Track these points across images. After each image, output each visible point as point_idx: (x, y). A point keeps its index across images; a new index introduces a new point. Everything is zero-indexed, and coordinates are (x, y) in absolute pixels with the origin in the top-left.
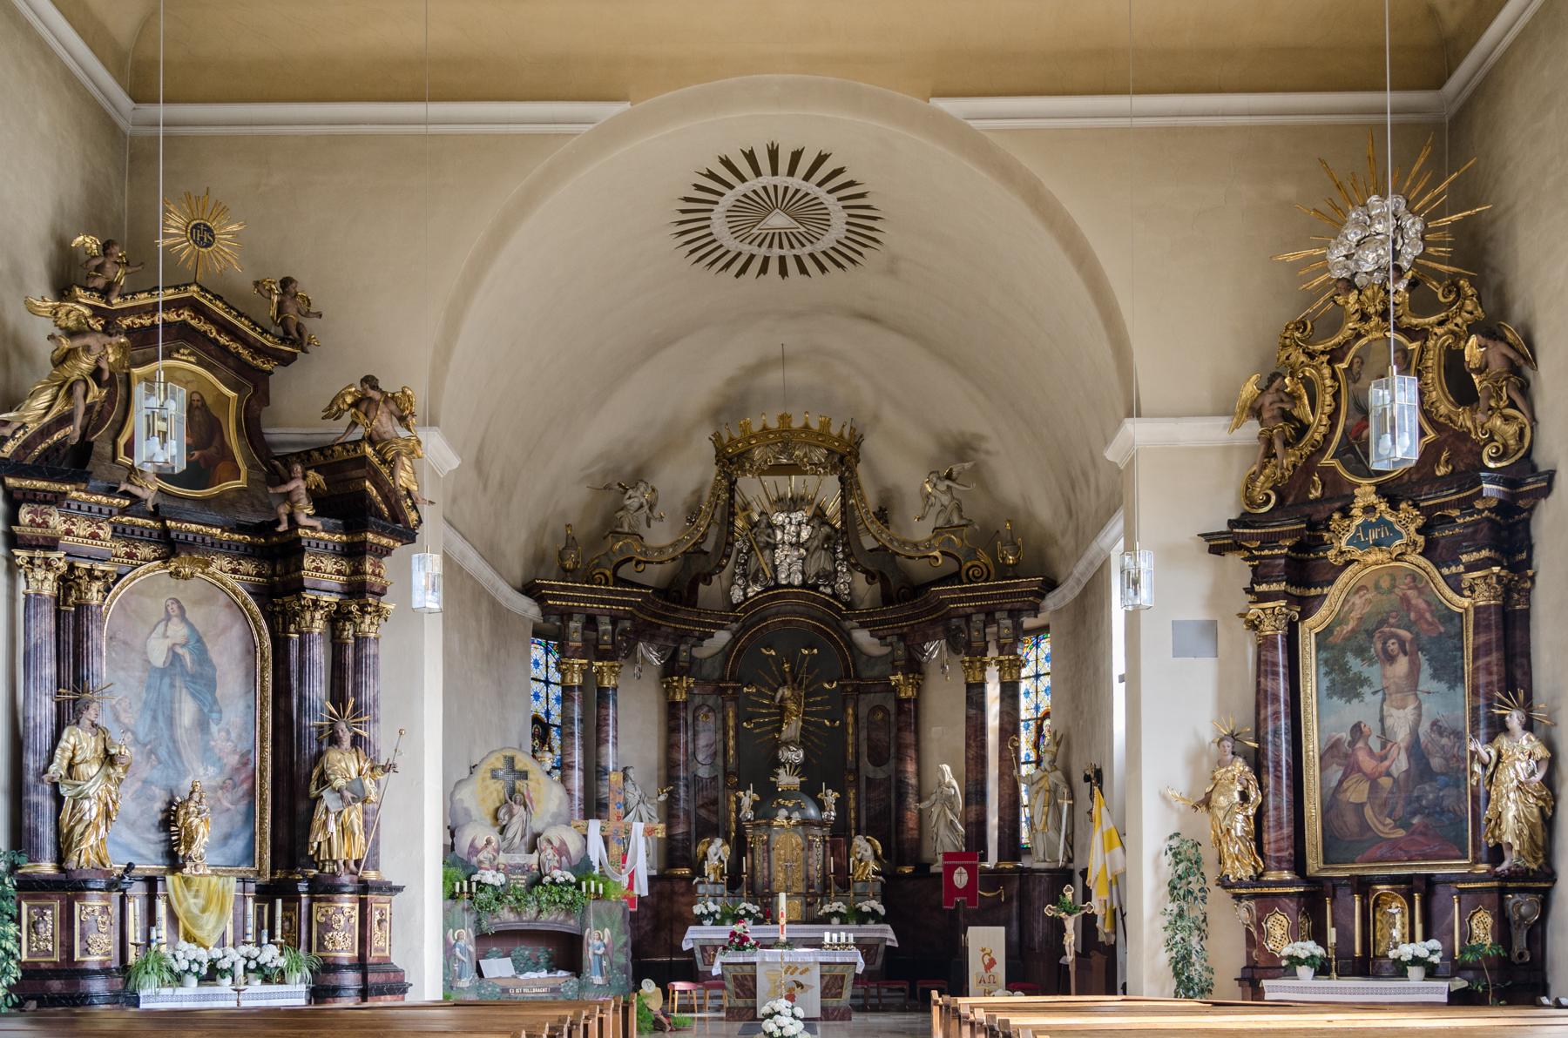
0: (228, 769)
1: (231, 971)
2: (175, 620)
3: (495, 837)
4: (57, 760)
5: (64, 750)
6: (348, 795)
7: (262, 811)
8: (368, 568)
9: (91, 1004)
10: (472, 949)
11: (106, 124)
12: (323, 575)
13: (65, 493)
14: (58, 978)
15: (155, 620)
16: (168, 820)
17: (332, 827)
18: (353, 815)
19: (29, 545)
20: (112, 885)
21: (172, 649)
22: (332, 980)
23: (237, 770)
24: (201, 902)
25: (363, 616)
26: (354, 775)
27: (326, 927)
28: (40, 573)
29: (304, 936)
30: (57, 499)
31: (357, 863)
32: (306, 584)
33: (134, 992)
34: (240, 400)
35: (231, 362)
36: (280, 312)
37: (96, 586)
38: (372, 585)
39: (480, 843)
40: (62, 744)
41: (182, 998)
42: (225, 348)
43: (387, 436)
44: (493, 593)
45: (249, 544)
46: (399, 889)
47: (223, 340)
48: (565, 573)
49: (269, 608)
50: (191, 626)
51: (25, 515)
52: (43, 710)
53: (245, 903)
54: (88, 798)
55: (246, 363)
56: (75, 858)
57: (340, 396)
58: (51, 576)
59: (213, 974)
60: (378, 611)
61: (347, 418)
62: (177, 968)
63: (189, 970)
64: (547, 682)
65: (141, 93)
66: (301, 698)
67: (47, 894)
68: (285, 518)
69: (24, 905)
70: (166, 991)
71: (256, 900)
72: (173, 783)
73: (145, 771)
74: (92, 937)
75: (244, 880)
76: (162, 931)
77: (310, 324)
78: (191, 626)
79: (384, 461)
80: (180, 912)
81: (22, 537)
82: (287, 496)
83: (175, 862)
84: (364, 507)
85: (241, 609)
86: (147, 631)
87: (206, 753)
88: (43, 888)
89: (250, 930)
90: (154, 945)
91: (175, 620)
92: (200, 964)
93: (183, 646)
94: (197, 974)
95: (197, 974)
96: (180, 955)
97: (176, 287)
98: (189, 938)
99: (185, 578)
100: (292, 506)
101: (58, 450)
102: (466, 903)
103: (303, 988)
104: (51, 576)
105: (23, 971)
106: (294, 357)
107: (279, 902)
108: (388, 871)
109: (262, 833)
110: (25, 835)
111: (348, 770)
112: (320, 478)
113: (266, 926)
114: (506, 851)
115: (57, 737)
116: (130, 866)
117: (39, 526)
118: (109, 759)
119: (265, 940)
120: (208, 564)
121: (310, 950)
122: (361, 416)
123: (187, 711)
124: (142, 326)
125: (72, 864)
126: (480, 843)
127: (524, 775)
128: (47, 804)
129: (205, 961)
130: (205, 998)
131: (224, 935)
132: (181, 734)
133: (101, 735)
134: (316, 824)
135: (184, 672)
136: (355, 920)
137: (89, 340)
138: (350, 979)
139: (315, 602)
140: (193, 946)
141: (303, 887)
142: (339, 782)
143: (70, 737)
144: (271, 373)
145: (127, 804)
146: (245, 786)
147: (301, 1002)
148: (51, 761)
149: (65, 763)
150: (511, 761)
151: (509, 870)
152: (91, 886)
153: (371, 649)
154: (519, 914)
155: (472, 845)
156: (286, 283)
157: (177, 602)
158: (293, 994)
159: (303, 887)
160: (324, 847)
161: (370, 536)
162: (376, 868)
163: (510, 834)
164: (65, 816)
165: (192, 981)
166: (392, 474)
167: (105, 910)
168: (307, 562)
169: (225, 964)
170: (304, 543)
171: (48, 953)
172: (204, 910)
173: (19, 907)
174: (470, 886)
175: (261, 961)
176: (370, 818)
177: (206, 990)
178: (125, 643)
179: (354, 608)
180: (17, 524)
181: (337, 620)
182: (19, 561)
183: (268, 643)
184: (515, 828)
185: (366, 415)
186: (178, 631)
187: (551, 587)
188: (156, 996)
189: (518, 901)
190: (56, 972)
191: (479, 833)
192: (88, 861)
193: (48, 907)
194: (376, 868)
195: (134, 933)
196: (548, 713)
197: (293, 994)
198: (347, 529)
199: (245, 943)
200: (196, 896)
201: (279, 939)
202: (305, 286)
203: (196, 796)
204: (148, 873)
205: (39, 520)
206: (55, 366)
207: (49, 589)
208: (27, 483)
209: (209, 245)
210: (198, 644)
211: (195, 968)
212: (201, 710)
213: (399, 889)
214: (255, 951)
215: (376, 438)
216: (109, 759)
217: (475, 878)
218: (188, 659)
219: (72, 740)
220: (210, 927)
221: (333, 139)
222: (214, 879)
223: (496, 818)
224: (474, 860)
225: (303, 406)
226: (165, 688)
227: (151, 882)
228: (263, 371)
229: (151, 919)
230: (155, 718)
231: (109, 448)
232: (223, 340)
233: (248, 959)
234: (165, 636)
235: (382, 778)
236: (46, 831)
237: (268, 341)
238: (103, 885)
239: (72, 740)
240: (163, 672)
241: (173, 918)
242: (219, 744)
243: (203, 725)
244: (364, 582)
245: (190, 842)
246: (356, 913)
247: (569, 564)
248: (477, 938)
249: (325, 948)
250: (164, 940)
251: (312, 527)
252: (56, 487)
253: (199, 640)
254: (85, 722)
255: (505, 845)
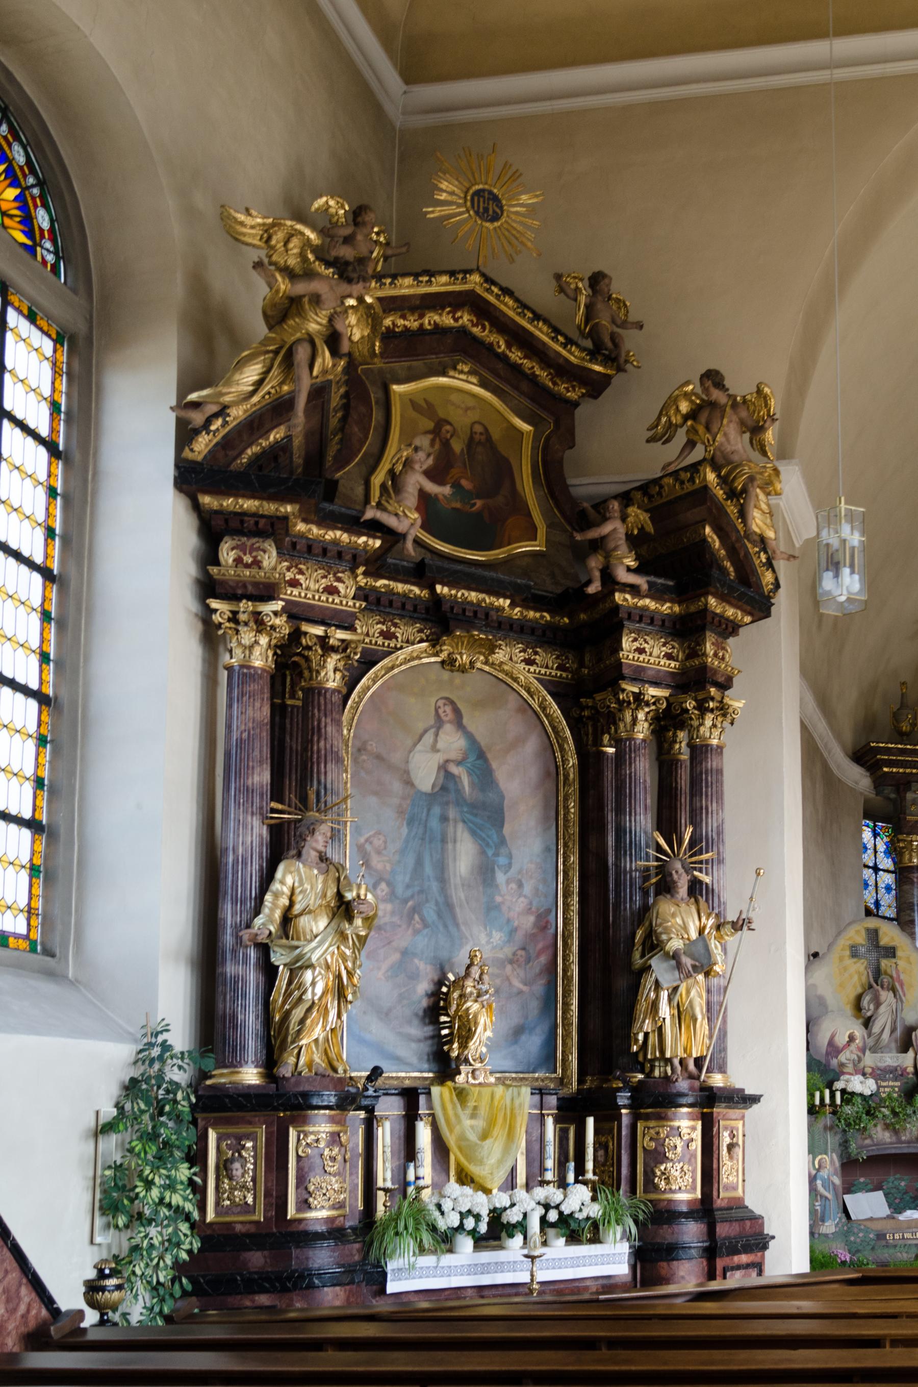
0: (519, 936)
1: (522, 1226)
2: (448, 727)
3: (859, 1032)
4: (266, 910)
5: (277, 895)
6: (687, 962)
7: (567, 1036)
8: (709, 648)
9: (311, 1286)
10: (837, 1181)
11: (363, 97)
12: (646, 653)
13: (285, 518)
14: (260, 1247)
15: (421, 726)
16: (436, 1007)
17: (665, 1010)
18: (693, 993)
19: (232, 596)
20: (348, 1100)
21: (443, 768)
22: (666, 1234)
23: (532, 937)
24: (480, 1123)
25: (702, 716)
26: (694, 935)
27: (658, 1156)
28: (247, 636)
29: (625, 1171)
30: (272, 529)
31: (699, 1062)
32: (626, 671)
33: (378, 1265)
34: (536, 436)
35: (525, 386)
36: (588, 317)
37: (332, 661)
38: (715, 671)
39: (842, 1040)
40: (276, 886)
41: (450, 1271)
42: (516, 368)
43: (736, 458)
44: (826, 755)
45: (548, 625)
46: (754, 1099)
47: (515, 356)
48: (902, 736)
49: (575, 713)
50: (470, 737)
51: (227, 553)
52: (248, 836)
53: (543, 1124)
54: (311, 966)
55: (544, 389)
56: (292, 1060)
57: (673, 401)
58: (264, 640)
59: (497, 1231)
60: (723, 710)
61: (681, 437)
62: (442, 1224)
63: (461, 1227)
64: (876, 869)
65: (412, 73)
66: (620, 831)
67: (248, 1115)
68: (597, 574)
69: (212, 1135)
70: (428, 1261)
71: (557, 1120)
72: (444, 954)
73: (404, 939)
74: (315, 1180)
75: (541, 1092)
76: (425, 1167)
77: (631, 341)
78: (470, 737)
79: (732, 494)
80: (451, 1140)
81: (223, 583)
82: (598, 545)
83: (445, 1067)
84: (703, 562)
85: (536, 716)
86: (409, 742)
87: (491, 909)
88: (241, 1108)
89: (549, 1164)
90: (411, 1189)
91: (448, 727)
92: (477, 1217)
93: (459, 763)
94: (473, 1232)
95: (473, 1232)
96: (447, 1205)
97: (452, 273)
98: (464, 1178)
99: (462, 670)
100: (607, 556)
101: (276, 458)
102: (828, 1119)
103: (624, 1248)
104: (264, 640)
105: (204, 1240)
106: (606, 381)
107: (590, 1121)
108: (737, 1075)
109: (567, 978)
110: (218, 1026)
111: (685, 928)
112: (644, 517)
113: (571, 1155)
114: (875, 1049)
115: (267, 878)
116: (376, 1072)
117: (247, 566)
118: (343, 909)
119: (571, 1177)
120: (492, 650)
121: (633, 1190)
122: (701, 429)
123: (464, 855)
124: (406, 329)
125: (285, 1071)
126: (842, 1040)
127: (891, 952)
128: (252, 978)
129: (484, 1213)
130: (485, 1269)
131: (513, 1170)
132: (458, 895)
133: (333, 874)
134: (642, 1006)
135: (460, 801)
136: (697, 1146)
137: (316, 286)
138: (691, 1232)
139: (638, 697)
140: (468, 1190)
141: (623, 1098)
142: (675, 944)
143: (287, 877)
144: (576, 404)
145: (373, 975)
146: (544, 959)
147: (621, 1268)
148: (257, 912)
149: (278, 914)
150: (873, 934)
151: (879, 1074)
152: (315, 1101)
153: (712, 763)
154: (896, 1132)
155: (831, 1043)
156: (597, 280)
157: (452, 703)
158: (611, 1259)
159: (623, 1098)
160: (653, 1039)
161: (712, 601)
162: (722, 1070)
163: (876, 1029)
164: (277, 995)
165: (466, 1244)
166: (743, 514)
167: (335, 1139)
168: (627, 643)
169: (513, 1216)
170: (623, 614)
171: (247, 1209)
172: (484, 1136)
173: (204, 1138)
174: (833, 1096)
175: (566, 1209)
176: (715, 998)
177: (486, 1256)
178: (379, 757)
179: (690, 704)
180: (217, 563)
181: (665, 729)
182: (216, 618)
183: (572, 761)
184: (883, 1020)
185: (708, 428)
186: (452, 742)
187: (888, 751)
188: (412, 1273)
189: (895, 1114)
190: (257, 1238)
191: (842, 1027)
192: (310, 1064)
193: (248, 1137)
194: (722, 1070)
195: (384, 1176)
196: (877, 904)
197: (611, 1259)
198: (680, 593)
199: (543, 1183)
200: (473, 1116)
201: (590, 1176)
202: (618, 287)
203: (475, 972)
204: (407, 1083)
205: (248, 559)
206: (271, 328)
207: (261, 659)
208: (228, 503)
209: (495, 218)
210: (479, 758)
211: (470, 1223)
212: (483, 853)
213: (754, 1099)
214: (553, 1194)
215: (720, 460)
216: (343, 909)
217: (839, 1085)
218: (466, 781)
219: (289, 880)
220: (492, 1160)
221: (658, 108)
222: (500, 1090)
223: (858, 1006)
224: (834, 1062)
225: (621, 445)
226: (434, 823)
227: (410, 1096)
228: (567, 401)
229: (410, 1152)
230: (419, 862)
231: (360, 490)
232: (515, 356)
233: (547, 1207)
234: (434, 749)
235: (732, 940)
236: (250, 1020)
237: (573, 356)
238: (333, 1100)
239: (289, 880)
240: (432, 798)
241: (441, 1148)
242: (508, 900)
243: (485, 872)
244: (704, 668)
245: (466, 1035)
246: (698, 1135)
247: (905, 727)
248: (844, 1166)
249: (656, 1188)
250: (427, 1181)
251: (637, 593)
252: (270, 508)
253: (481, 755)
254: (310, 854)
255: (870, 1042)
